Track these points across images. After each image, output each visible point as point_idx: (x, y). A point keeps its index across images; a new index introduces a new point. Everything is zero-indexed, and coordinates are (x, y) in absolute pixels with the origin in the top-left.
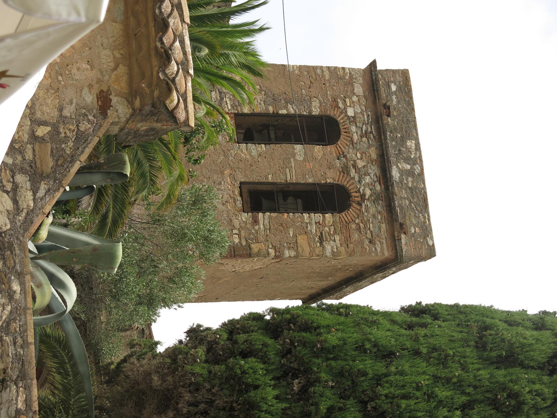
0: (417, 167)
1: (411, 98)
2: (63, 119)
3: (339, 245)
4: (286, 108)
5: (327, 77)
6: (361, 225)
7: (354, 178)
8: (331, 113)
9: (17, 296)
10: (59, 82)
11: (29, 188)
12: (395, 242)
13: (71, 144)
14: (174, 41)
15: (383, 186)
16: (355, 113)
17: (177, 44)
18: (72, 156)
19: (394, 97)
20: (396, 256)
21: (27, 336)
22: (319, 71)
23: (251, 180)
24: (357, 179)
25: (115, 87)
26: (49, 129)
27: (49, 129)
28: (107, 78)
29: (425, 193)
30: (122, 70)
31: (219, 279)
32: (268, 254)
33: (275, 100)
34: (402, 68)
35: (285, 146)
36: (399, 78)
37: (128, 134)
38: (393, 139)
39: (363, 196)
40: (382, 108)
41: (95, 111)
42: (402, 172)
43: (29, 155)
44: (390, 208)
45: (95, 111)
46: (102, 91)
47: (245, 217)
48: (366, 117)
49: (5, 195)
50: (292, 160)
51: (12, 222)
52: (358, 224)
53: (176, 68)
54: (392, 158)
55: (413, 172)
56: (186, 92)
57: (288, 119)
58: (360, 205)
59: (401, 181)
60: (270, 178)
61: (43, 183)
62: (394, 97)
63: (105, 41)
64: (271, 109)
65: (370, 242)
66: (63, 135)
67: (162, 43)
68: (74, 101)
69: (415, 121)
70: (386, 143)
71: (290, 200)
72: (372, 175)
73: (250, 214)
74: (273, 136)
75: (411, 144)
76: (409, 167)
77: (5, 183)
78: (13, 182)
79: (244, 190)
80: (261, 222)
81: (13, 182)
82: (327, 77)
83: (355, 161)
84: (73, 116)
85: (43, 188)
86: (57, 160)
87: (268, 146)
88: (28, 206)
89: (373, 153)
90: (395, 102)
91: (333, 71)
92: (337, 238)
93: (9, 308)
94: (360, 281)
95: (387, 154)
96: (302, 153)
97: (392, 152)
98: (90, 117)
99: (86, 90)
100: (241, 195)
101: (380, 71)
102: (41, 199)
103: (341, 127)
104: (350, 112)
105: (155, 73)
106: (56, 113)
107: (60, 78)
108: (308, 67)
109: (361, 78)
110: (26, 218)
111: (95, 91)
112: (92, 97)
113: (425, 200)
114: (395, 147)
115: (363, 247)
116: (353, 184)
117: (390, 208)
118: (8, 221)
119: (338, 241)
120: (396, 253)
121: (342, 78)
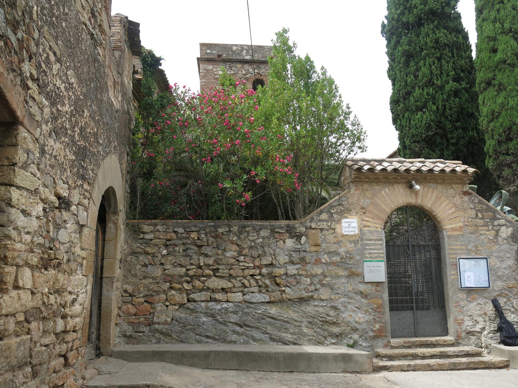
0: (245, 47)
1: (213, 44)
5: (205, 80)
13: (483, 206)
19: (213, 52)
22: (203, 84)
38: (232, 56)
39: (258, 73)
42: (247, 54)
43: (488, 220)
51: (510, 227)
58: (261, 75)
62: (213, 52)
69: (224, 45)
75: (234, 48)
76: (245, 51)
82: (205, 80)
85: (498, 216)
89: (239, 66)
97: (238, 57)
99: (463, 199)
111: (463, 196)
113: (259, 46)
114: (236, 56)
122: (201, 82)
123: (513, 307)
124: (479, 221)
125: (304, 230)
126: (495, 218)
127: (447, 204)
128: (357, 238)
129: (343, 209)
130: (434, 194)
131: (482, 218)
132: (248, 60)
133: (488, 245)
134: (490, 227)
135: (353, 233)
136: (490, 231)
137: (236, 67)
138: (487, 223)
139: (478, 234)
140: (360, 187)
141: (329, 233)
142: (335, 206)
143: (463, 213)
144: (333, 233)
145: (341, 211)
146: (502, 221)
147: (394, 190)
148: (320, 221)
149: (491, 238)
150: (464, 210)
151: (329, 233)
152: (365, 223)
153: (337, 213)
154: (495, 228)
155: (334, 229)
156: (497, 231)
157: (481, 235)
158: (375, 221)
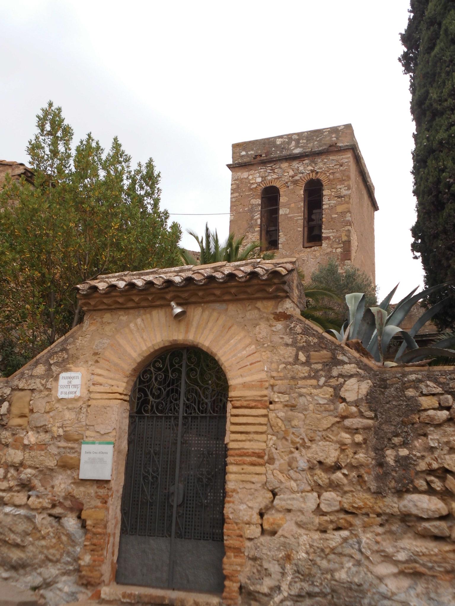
2: (294, 344)
3: (344, 186)
4: (256, 220)
6: (330, 172)
7: (301, 177)
8: (259, 192)
9: (420, 377)
10: (268, 346)
11: (342, 367)
12: (340, 150)
13: (311, 339)
14: (240, 270)
15: (306, 158)
16: (259, 177)
17: (242, 268)
18: (319, 338)
19: (249, 153)
20: (351, 149)
21: (449, 371)
22: (234, 200)
23: (302, 241)
24: (301, 175)
25: (270, 309)
26: (300, 353)
27: (300, 353)
28: (265, 315)
29: (310, 131)
30: (259, 304)
31: (362, 262)
32: (349, 230)
33: (251, 227)
34: (231, 148)
35: (280, 219)
36: (238, 150)
37: (300, 302)
39: (312, 171)
40: (256, 160)
41: (288, 323)
42: (297, 146)
43: (319, 366)
44: (320, 154)
45: (288, 323)
46: (274, 318)
47: (325, 244)
48: (262, 170)
49: (347, 383)
50: (289, 216)
52: (330, 174)
53: (259, 269)
54: (288, 153)
55: (297, 139)
56: (273, 264)
57: (263, 219)
58: (317, 173)
59: (302, 147)
60: (300, 229)
61: (338, 358)
62: (249, 153)
63: (240, 316)
64: (258, 229)
65: (341, 166)
66: (305, 344)
67: (242, 277)
68: (281, 336)
70: (279, 157)
71: (313, 217)
72: (299, 166)
73: (323, 242)
74: (273, 228)
77: (338, 383)
78: (338, 377)
79: (307, 245)
80: (328, 235)
81: (338, 377)
82: (237, 194)
83: (290, 176)
84: (292, 337)
85: (340, 357)
86: (322, 348)
87: (280, 231)
88: (354, 368)
89: (285, 165)
90: (252, 152)
91: (233, 191)
92: (339, 187)
93: (428, 382)
94: (365, 173)
95: (285, 156)
96: (284, 209)
97: (285, 153)
98: (292, 325)
99: (274, 329)
100: (311, 247)
101: (233, 162)
102: (349, 358)
103: (269, 185)
104: (259, 180)
105: (262, 283)
106: (290, 348)
107: (266, 345)
108: (231, 206)
109: (238, 174)
110: (363, 369)
111: (275, 323)
112: (279, 325)
115: (345, 171)
116: (304, 177)
117: (320, 154)
118: (365, 382)
119: (341, 186)
120: (348, 149)
121: (238, 185)
122: (231, 198)
123: (360, 551)
124: (300, 367)
125: (8, 393)
126: (335, 362)
127: (241, 340)
128: (80, 403)
129: (66, 356)
130: (220, 322)
131: (307, 363)
132: (297, 154)
133: (314, 415)
134: (322, 380)
135: (72, 396)
136: (321, 387)
137: (280, 168)
138: (317, 371)
139: (295, 395)
140: (99, 320)
141: (41, 395)
142: (56, 352)
143: (269, 354)
144: (47, 396)
145: (64, 360)
146: (350, 368)
147: (152, 320)
148: (32, 376)
149: (321, 402)
150: (273, 348)
151: (41, 395)
152: (96, 378)
153: (57, 364)
154: (333, 382)
155: (50, 390)
156: (337, 389)
157: (301, 395)
158: (112, 375)
